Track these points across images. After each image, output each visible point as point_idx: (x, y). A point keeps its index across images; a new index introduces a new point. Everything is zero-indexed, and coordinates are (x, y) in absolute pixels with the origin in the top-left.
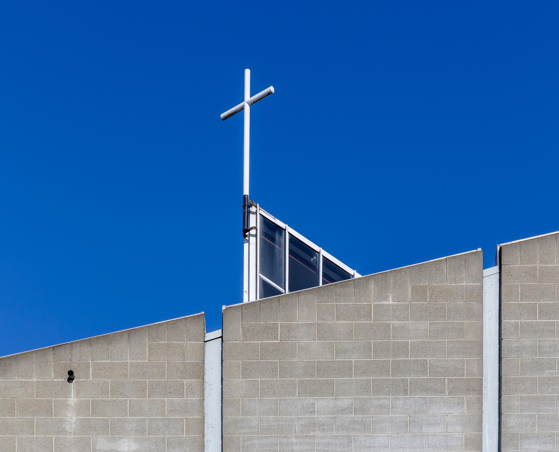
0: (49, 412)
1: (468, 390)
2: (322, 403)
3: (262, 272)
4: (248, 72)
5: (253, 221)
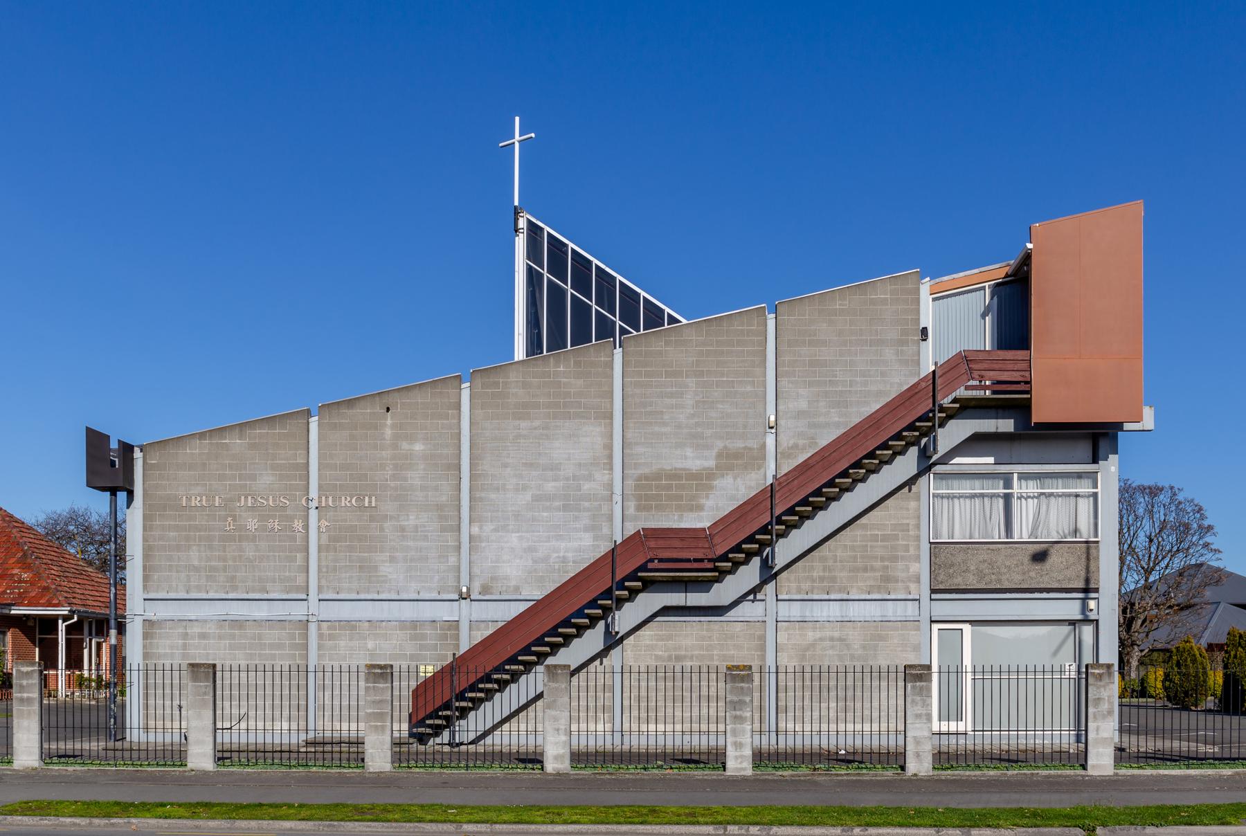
0: (376, 429)
1: (604, 418)
2: (524, 424)
3: (528, 258)
4: (517, 119)
5: (522, 223)
